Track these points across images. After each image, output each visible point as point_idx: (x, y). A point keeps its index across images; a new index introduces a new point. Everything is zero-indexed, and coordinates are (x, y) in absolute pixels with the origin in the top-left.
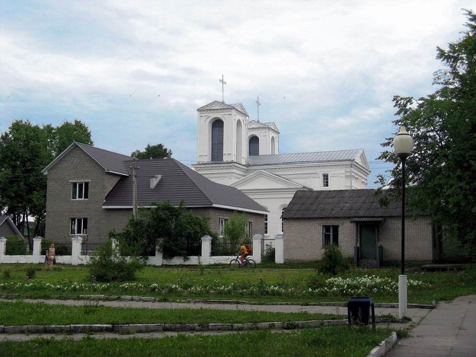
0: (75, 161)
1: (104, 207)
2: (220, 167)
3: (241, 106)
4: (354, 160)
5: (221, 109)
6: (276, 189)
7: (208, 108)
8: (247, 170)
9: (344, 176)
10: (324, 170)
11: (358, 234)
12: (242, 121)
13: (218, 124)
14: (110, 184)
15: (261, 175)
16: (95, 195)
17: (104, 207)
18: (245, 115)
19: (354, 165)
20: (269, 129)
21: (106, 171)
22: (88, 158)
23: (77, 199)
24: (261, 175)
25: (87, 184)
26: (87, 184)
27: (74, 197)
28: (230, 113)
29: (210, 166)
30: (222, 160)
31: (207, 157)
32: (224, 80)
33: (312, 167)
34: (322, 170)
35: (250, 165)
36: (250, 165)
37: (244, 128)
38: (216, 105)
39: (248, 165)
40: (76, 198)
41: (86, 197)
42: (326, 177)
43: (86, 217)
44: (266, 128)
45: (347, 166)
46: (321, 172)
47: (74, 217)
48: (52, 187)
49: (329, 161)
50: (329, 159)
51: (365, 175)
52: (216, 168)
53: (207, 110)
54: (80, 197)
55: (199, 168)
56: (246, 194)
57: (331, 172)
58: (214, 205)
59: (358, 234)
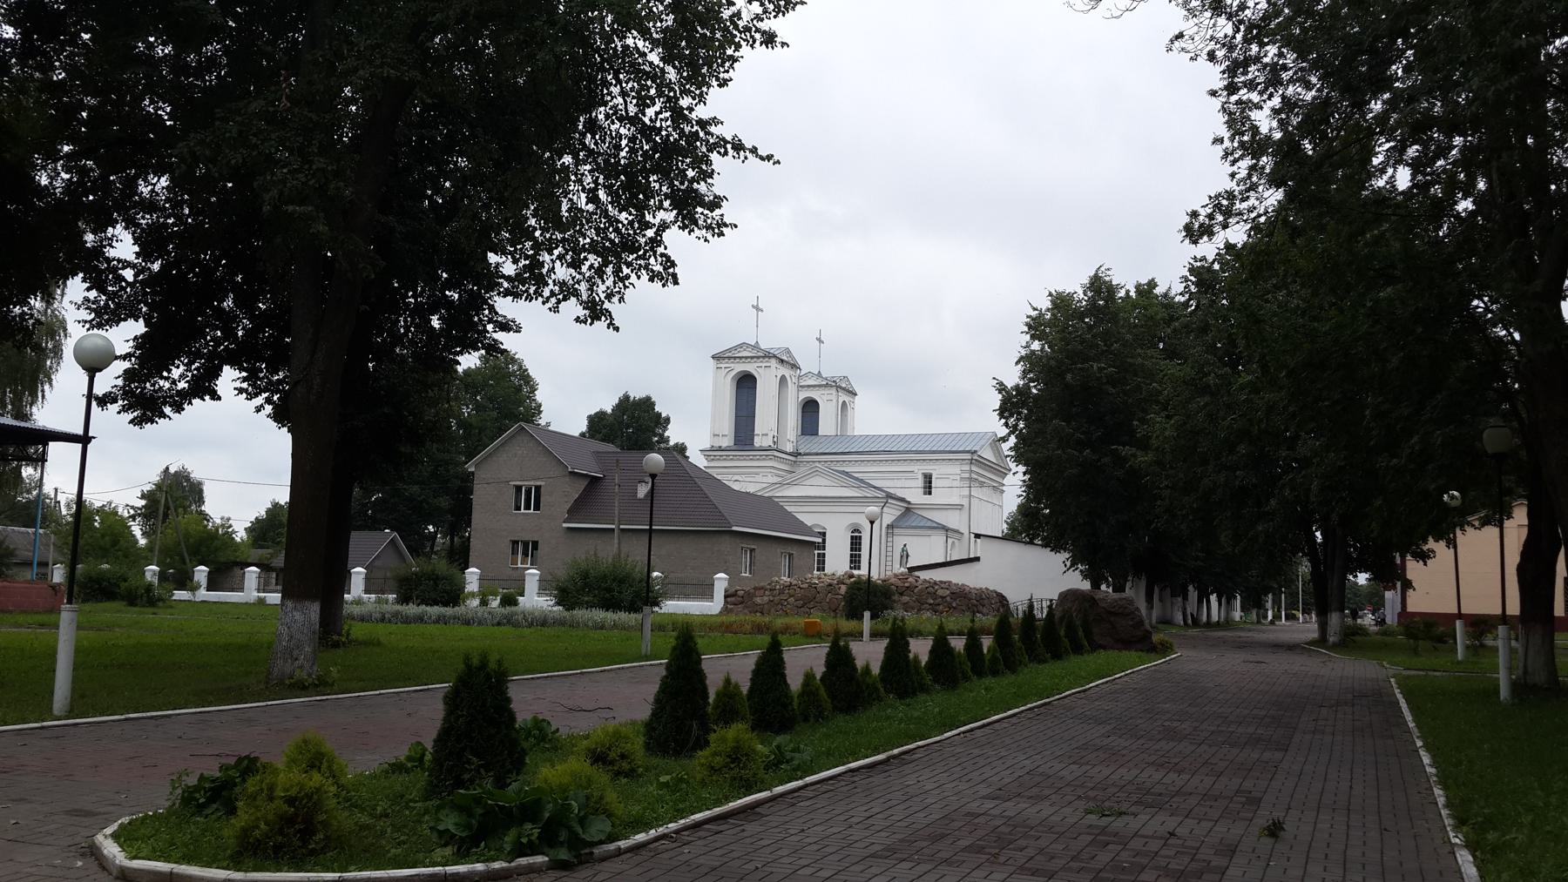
0: (520, 452)
1: (565, 525)
2: (749, 456)
3: (788, 351)
4: (975, 452)
5: (752, 358)
6: (816, 497)
7: (730, 354)
8: (795, 462)
9: (958, 477)
10: (926, 467)
11: (490, 455)
12: (788, 379)
13: (746, 383)
14: (576, 490)
15: (816, 472)
16: (553, 506)
17: (565, 525)
18: (795, 366)
19: (976, 460)
20: (838, 388)
21: (570, 470)
22: (541, 448)
23: (522, 511)
24: (817, 473)
25: (538, 488)
26: (538, 488)
27: (518, 508)
28: (768, 365)
29: (734, 453)
30: (753, 444)
31: (726, 438)
32: (760, 307)
33: (886, 461)
34: (921, 467)
35: (800, 454)
36: (800, 454)
37: (791, 388)
38: (745, 350)
39: (796, 454)
40: (520, 510)
41: (537, 507)
42: (928, 479)
43: (536, 540)
44: (832, 386)
45: (964, 462)
46: (920, 469)
47: (516, 539)
48: (481, 496)
49: (934, 452)
50: (935, 449)
51: (1001, 477)
52: (742, 458)
53: (729, 358)
54: (528, 507)
55: (712, 457)
56: (781, 504)
57: (936, 470)
58: (734, 528)
59: (490, 455)
